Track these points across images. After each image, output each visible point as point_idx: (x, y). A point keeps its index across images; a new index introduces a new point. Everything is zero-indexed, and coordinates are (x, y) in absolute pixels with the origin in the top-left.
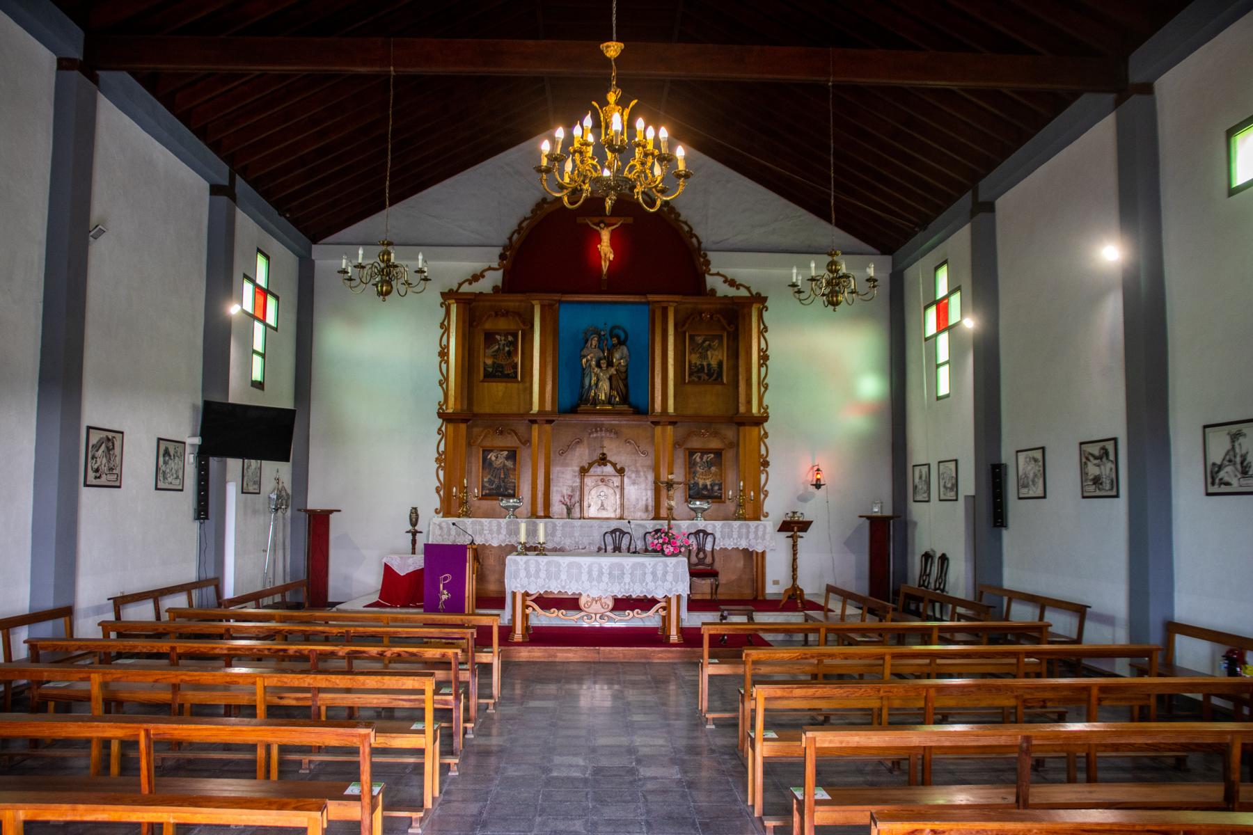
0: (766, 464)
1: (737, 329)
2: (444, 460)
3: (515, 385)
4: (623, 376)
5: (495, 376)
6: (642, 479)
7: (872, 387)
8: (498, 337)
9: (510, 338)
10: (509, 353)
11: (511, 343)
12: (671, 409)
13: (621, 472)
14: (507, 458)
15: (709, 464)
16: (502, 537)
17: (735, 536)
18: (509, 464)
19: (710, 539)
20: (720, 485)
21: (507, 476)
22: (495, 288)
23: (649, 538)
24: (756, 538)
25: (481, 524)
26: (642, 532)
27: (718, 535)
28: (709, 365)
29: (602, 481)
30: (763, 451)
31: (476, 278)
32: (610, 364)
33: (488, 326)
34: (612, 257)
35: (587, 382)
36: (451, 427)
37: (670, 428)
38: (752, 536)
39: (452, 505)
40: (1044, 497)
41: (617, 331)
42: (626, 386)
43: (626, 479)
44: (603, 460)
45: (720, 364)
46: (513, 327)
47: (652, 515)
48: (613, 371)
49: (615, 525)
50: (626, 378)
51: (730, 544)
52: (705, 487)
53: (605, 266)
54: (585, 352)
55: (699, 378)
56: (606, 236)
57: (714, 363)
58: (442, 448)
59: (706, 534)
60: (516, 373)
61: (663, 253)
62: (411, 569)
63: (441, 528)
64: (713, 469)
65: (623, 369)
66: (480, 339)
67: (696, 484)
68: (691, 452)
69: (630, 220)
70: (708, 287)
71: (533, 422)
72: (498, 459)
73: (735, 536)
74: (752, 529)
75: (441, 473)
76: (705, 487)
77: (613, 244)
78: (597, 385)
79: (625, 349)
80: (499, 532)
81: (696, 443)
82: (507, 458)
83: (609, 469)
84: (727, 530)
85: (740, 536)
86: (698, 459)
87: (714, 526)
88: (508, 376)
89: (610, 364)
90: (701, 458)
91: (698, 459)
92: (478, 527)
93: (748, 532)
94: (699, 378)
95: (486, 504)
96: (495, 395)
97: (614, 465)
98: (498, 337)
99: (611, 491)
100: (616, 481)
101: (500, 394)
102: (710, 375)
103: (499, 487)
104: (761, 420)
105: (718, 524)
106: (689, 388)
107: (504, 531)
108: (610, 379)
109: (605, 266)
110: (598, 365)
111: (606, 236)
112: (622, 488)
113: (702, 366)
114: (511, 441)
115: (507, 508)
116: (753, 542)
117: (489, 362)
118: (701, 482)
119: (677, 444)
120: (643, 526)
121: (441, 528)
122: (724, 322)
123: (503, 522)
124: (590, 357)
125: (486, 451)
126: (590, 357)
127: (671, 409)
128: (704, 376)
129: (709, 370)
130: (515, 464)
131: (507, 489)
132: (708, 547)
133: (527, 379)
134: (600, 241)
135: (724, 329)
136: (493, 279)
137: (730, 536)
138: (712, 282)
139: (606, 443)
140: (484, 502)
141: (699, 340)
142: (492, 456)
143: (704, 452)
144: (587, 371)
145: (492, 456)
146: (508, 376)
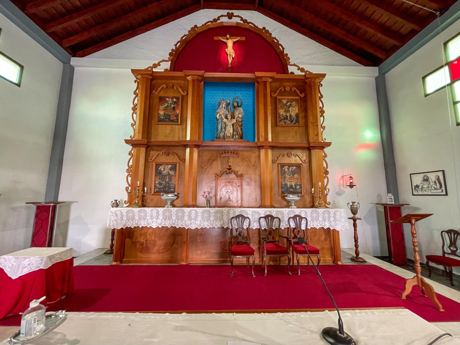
0: (327, 172)
1: (305, 96)
2: (132, 171)
3: (177, 127)
4: (240, 124)
5: (165, 121)
6: (253, 183)
7: (371, 135)
8: (167, 99)
9: (175, 100)
10: (174, 108)
11: (175, 102)
12: (270, 139)
13: (240, 176)
14: (171, 169)
15: (294, 173)
16: (159, 221)
17: (321, 219)
18: (172, 173)
19: (303, 222)
20: (301, 185)
21: (170, 179)
22: (166, 70)
23: (262, 220)
24: (335, 220)
25: (145, 212)
26: (257, 217)
27: (309, 219)
28: (290, 115)
29: (229, 182)
30: (325, 165)
31: (155, 66)
32: (233, 117)
33: (162, 94)
34: (234, 56)
35: (220, 127)
36: (135, 149)
37: (270, 151)
38: (332, 219)
39: (140, 198)
40: (413, 195)
41: (237, 100)
42: (242, 130)
43: (244, 184)
44: (230, 170)
45: (297, 116)
46: (176, 95)
47: (259, 204)
48: (234, 121)
49: (238, 211)
50: (242, 126)
51: (317, 225)
52: (291, 186)
53: (230, 60)
54: (218, 111)
55: (285, 123)
56: (230, 43)
57: (293, 114)
58: (131, 163)
59: (301, 218)
60: (177, 119)
61: (262, 53)
62: (26, 271)
63: (116, 215)
64: (296, 176)
65: (240, 120)
66: (156, 101)
67: (286, 185)
68: (283, 165)
69: (243, 39)
70: (290, 71)
71: (186, 146)
72: (165, 169)
73: (321, 219)
74: (332, 215)
75: (130, 179)
76: (291, 186)
77: (234, 48)
78: (225, 128)
79: (241, 109)
80: (157, 218)
81: (286, 160)
82: (171, 169)
83: (233, 176)
84: (315, 215)
85: (324, 220)
86: (286, 170)
87: (306, 213)
88: (172, 121)
89: (233, 117)
90: (288, 169)
91: (286, 170)
92: (143, 214)
93: (329, 217)
94: (285, 123)
95: (156, 198)
96: (163, 133)
97: (236, 173)
98: (167, 99)
99: (235, 189)
100: (237, 181)
101: (168, 131)
102: (291, 121)
103: (165, 187)
104: (323, 146)
105: (309, 210)
106: (279, 129)
107: (161, 217)
108: (233, 125)
109: (230, 60)
110: (226, 118)
111: (230, 43)
112: (241, 186)
113: (287, 116)
114: (172, 159)
115: (166, 201)
116: (333, 223)
117: (162, 113)
118: (289, 184)
119: (273, 162)
120: (258, 213)
121: (116, 215)
122: (298, 92)
123: (161, 210)
124: (222, 112)
125: (158, 165)
126: (222, 112)
127: (270, 139)
128: (288, 122)
129: (291, 118)
130: (175, 173)
131: (170, 188)
132: (303, 227)
133: (184, 123)
134: (227, 47)
135: (298, 95)
136: (167, 65)
137: (317, 219)
138: (291, 69)
139: (231, 160)
140: (154, 196)
141: (284, 101)
142: (161, 168)
143: (290, 165)
144: (219, 122)
145: (161, 168)
146: (172, 121)
